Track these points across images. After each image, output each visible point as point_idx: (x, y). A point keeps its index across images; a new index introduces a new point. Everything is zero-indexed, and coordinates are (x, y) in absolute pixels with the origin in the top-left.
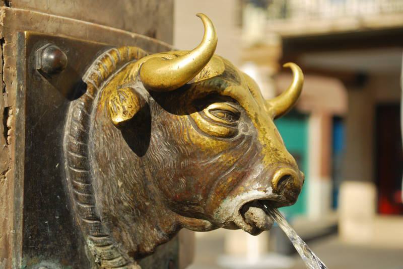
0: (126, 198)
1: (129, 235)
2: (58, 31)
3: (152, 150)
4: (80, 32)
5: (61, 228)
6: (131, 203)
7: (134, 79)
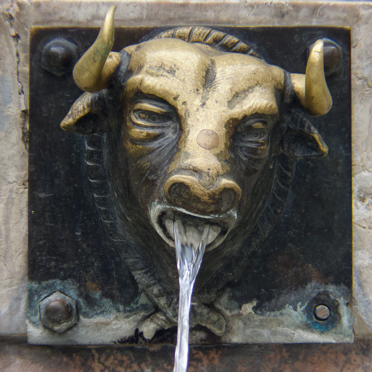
5: (84, 246)
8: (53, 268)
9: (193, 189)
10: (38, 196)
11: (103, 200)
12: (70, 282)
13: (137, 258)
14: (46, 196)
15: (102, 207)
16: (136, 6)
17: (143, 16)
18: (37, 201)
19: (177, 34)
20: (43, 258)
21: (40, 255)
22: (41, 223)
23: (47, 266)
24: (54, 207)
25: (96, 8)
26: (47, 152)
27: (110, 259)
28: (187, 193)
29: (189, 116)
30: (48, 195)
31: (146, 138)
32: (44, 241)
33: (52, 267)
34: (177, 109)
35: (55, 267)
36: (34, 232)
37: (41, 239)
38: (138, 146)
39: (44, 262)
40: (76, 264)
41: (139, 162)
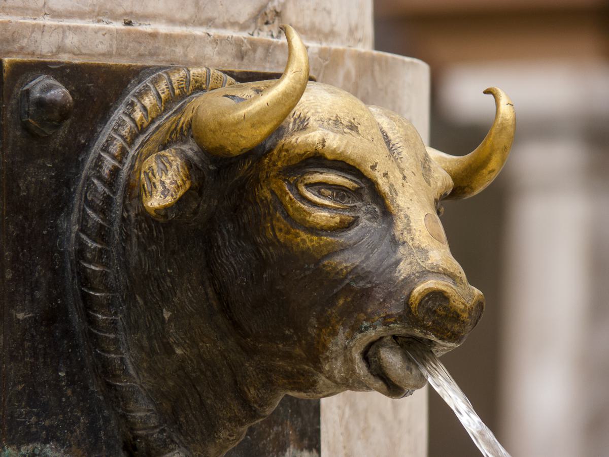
0: (177, 339)
1: (76, 281)
2: (60, 49)
3: (216, 254)
4: (100, 46)
5: (69, 392)
6: (188, 350)
7: (185, 133)
8: (34, 426)
9: (454, 302)
10: (16, 316)
11: (113, 323)
12: (54, 447)
13: (149, 411)
14: (25, 316)
15: (110, 334)
16: (105, 34)
17: (113, 50)
18: (15, 324)
19: (192, 77)
20: (22, 410)
21: (19, 407)
22: (19, 358)
23: (27, 422)
24: (35, 334)
25: (62, 36)
26: (25, 251)
27: (97, 413)
28: (445, 307)
29: (397, 195)
30: (28, 316)
31: (338, 226)
32: (24, 385)
33: (32, 424)
34: (378, 184)
35: (37, 423)
36: (12, 371)
37: (20, 383)
38: (325, 238)
39: (23, 416)
40: (59, 420)
41: (327, 262)
